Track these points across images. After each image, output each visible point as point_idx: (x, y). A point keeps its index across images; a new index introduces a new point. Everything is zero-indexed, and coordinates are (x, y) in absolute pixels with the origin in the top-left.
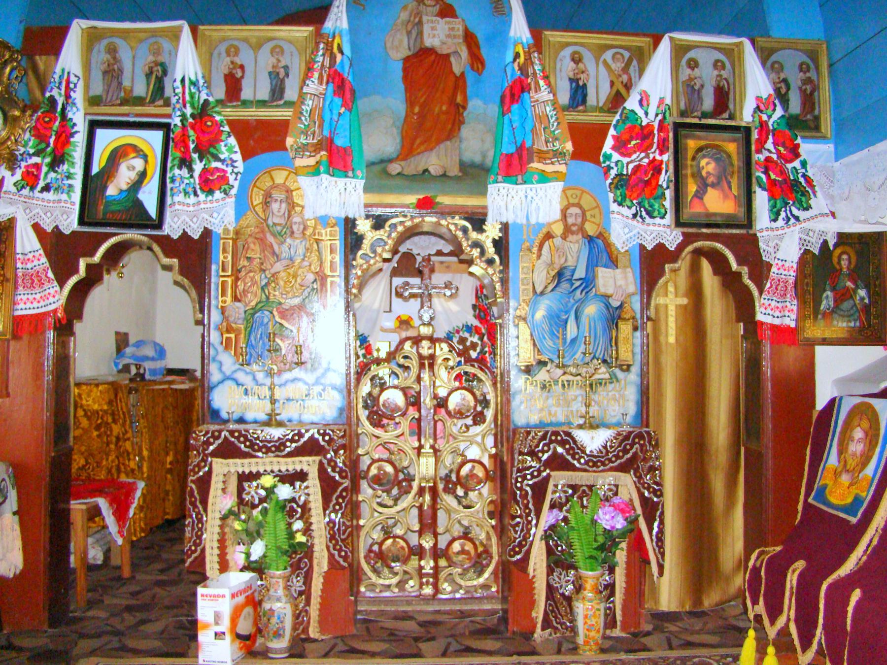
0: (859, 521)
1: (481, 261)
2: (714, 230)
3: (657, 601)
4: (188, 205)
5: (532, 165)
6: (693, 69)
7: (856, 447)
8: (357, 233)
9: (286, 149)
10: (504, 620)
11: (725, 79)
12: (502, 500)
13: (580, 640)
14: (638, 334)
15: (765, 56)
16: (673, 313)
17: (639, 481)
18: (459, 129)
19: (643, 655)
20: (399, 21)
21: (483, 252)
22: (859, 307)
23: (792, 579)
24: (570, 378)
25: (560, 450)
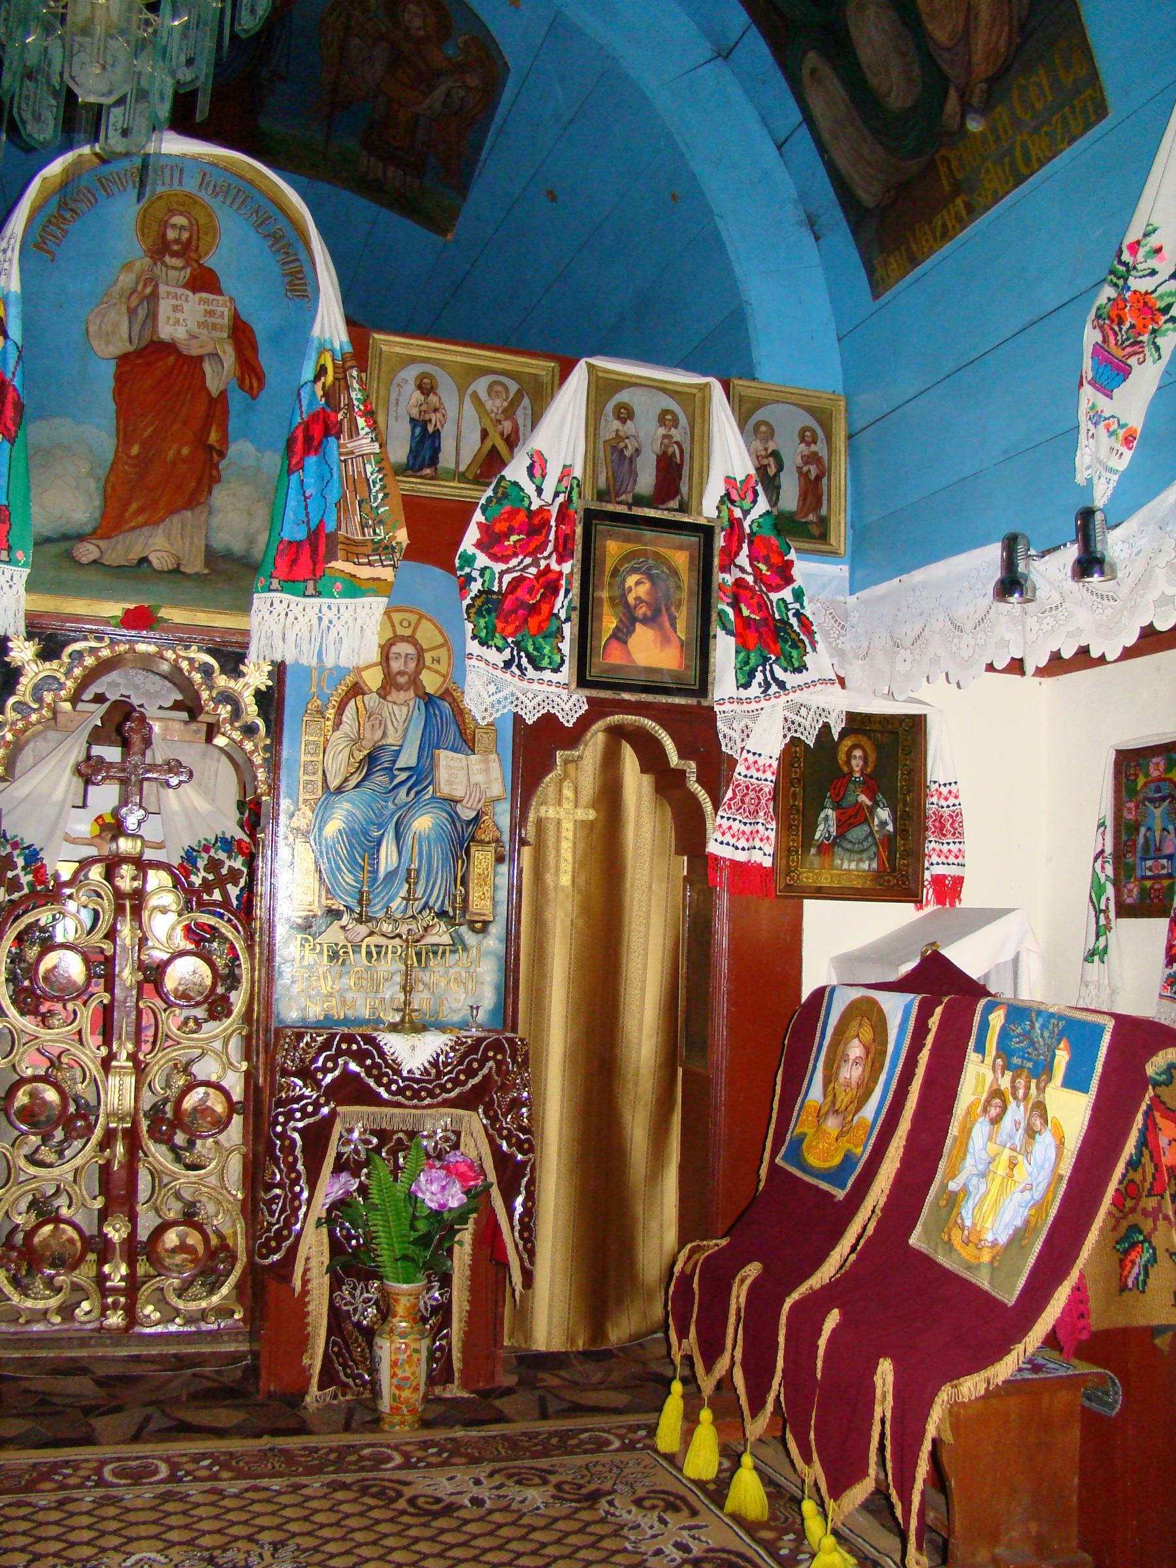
0: (848, 1195)
1: (234, 728)
2: (643, 697)
3: (528, 1334)
5: (333, 564)
6: (624, 422)
7: (851, 1073)
8: (9, 664)
10: (253, 1372)
11: (677, 443)
12: (255, 1155)
13: (385, 1405)
14: (504, 868)
15: (745, 412)
16: (570, 835)
17: (493, 1127)
18: (210, 492)
19: (494, 1430)
20: (117, 288)
21: (237, 713)
22: (877, 836)
23: (739, 1295)
24: (382, 941)
25: (353, 1066)
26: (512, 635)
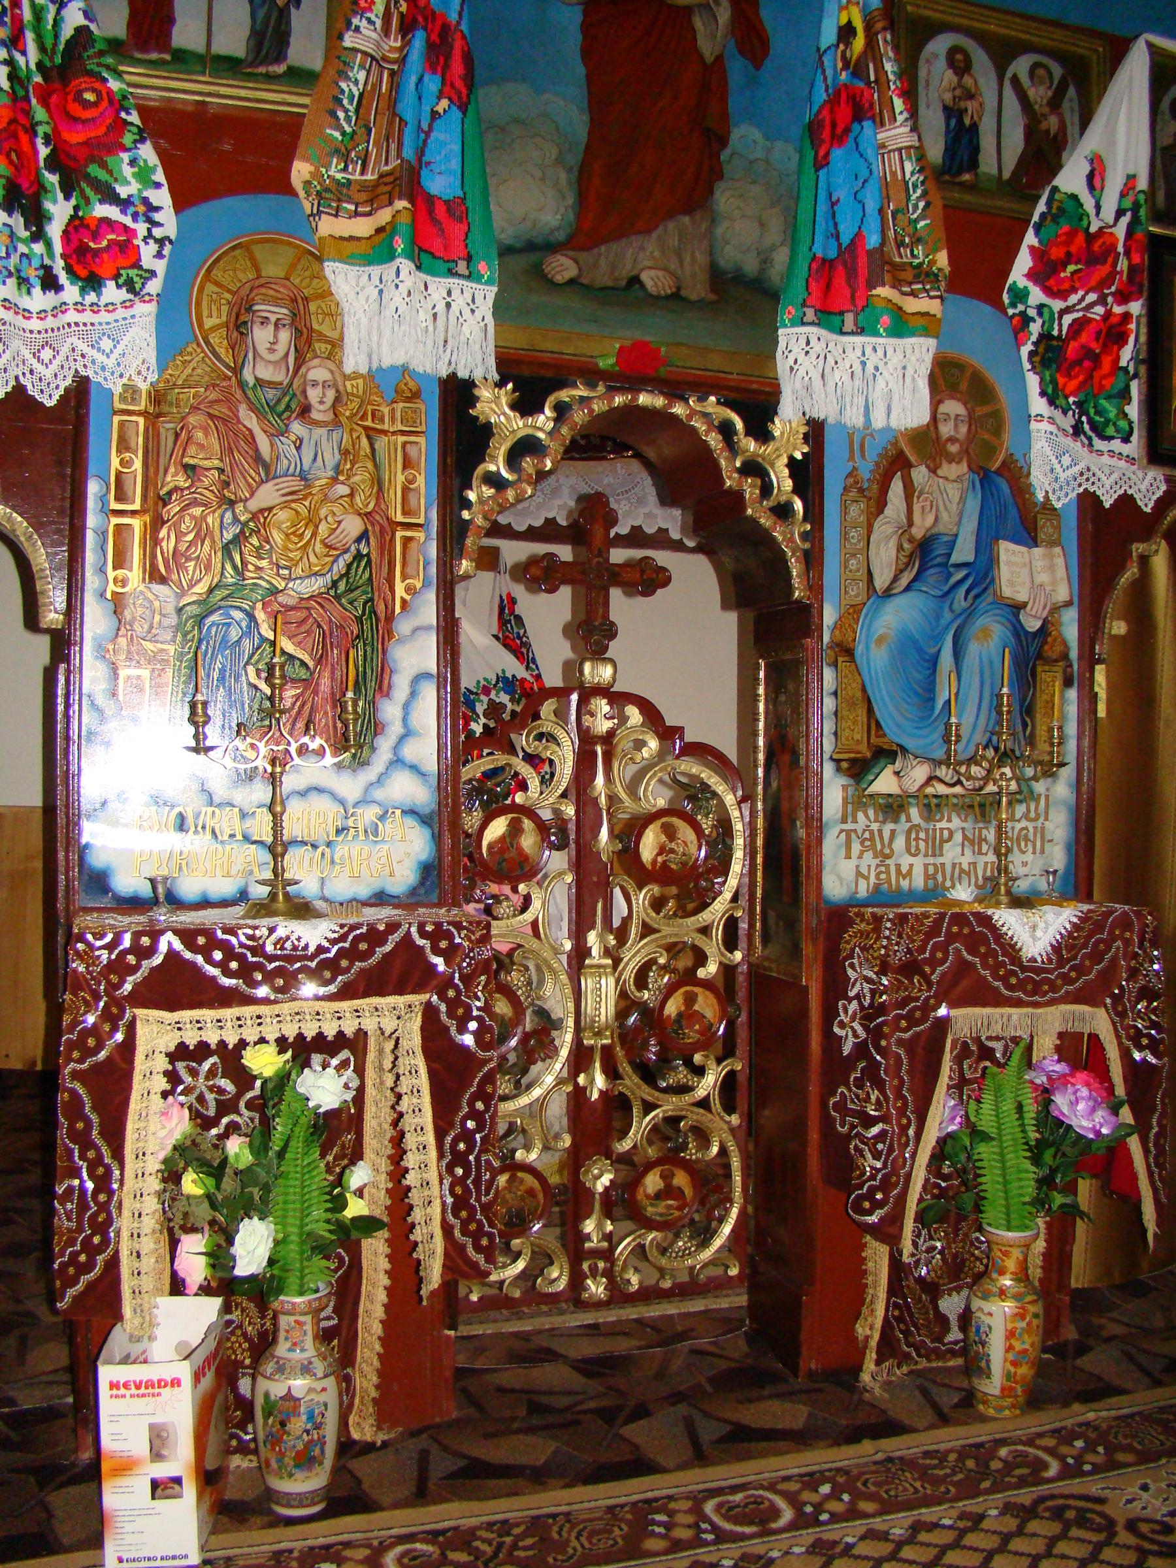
4: (27, 314)
8: (477, 418)
9: (290, 191)
18: (711, 191)
26: (1073, 394)
